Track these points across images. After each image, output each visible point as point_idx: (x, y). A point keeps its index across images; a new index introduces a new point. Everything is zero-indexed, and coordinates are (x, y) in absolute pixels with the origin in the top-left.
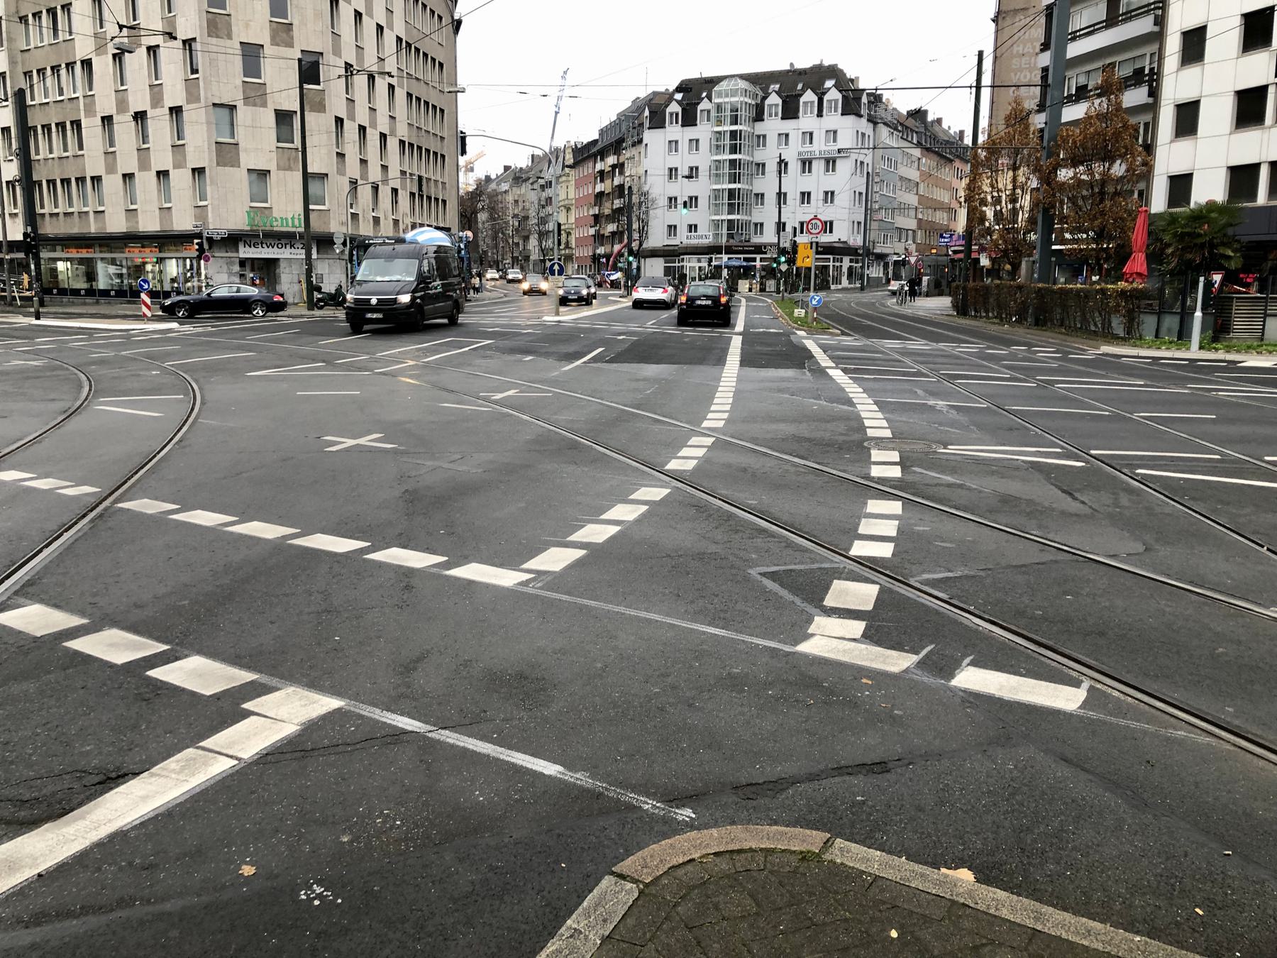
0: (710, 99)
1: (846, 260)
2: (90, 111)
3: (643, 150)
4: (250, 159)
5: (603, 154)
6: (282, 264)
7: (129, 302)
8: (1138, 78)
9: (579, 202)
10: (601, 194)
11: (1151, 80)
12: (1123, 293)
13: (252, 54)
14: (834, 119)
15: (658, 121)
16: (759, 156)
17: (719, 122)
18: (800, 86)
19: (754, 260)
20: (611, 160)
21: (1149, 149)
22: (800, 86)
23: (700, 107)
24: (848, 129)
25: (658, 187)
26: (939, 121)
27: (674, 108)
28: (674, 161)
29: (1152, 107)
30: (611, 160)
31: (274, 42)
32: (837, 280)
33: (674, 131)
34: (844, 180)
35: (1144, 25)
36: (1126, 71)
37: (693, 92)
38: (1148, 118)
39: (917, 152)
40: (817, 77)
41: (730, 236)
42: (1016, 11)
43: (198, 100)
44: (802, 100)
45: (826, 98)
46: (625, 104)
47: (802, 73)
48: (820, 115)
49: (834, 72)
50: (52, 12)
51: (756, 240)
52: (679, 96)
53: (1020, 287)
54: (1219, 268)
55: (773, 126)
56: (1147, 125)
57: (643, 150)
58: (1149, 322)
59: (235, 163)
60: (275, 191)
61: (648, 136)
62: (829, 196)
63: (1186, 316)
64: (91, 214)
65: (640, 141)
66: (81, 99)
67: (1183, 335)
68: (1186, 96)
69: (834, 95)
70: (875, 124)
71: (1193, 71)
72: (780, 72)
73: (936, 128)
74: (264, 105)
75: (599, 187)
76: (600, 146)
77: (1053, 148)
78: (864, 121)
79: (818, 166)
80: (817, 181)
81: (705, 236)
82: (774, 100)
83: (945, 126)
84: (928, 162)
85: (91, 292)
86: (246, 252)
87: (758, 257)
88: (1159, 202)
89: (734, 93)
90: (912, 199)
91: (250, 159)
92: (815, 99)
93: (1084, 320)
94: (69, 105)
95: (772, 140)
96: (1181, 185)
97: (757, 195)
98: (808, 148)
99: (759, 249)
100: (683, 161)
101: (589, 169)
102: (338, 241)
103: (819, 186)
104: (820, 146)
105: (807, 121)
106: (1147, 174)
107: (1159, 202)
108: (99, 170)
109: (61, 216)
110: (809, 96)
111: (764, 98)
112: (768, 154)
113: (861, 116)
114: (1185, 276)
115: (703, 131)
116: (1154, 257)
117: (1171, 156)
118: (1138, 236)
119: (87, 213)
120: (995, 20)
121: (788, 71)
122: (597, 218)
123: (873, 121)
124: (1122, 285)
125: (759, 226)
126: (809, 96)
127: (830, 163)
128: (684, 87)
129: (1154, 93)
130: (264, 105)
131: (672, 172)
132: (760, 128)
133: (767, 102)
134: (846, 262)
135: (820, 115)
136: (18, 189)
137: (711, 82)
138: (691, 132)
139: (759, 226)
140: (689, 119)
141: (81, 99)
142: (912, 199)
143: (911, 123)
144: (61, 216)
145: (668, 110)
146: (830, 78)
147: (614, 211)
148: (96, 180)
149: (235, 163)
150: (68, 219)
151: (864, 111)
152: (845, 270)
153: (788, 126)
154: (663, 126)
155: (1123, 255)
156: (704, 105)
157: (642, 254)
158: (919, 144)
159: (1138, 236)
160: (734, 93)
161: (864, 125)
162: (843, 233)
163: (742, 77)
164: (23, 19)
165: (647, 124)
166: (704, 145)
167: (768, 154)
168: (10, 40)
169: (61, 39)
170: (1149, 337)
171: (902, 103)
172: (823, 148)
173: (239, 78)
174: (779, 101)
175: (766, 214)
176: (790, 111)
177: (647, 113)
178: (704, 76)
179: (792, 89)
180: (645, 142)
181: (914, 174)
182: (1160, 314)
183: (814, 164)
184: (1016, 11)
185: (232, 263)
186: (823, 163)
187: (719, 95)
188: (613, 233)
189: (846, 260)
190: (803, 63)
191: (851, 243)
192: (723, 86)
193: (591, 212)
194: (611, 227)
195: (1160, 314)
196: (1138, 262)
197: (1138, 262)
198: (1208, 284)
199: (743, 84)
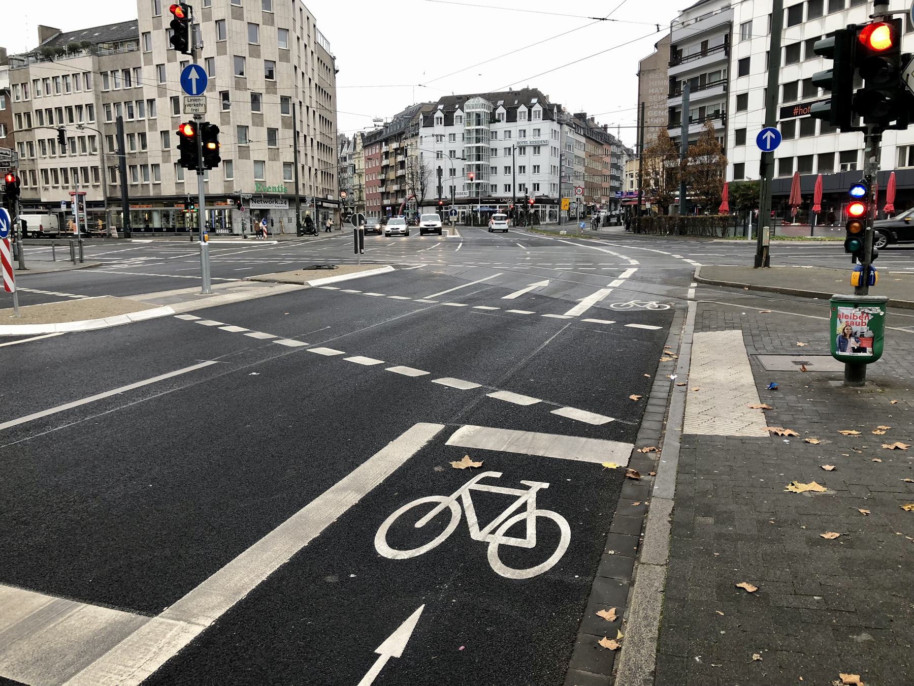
0: (462, 110)
1: (548, 209)
2: (153, 126)
3: (419, 140)
4: (255, 156)
5: (387, 141)
6: (271, 212)
7: (176, 235)
8: (716, 115)
9: (369, 172)
10: (387, 166)
11: (723, 117)
12: (721, 218)
13: (255, 99)
14: (538, 122)
15: (429, 122)
16: (493, 144)
17: (469, 124)
18: (516, 102)
19: (495, 207)
20: (395, 145)
21: (723, 151)
22: (516, 102)
23: (455, 114)
24: (547, 127)
25: (431, 164)
26: (593, 119)
27: (439, 114)
28: (439, 147)
29: (725, 129)
30: (395, 145)
31: (267, 93)
32: (544, 219)
33: (439, 129)
34: (546, 159)
35: (719, 90)
36: (711, 112)
37: (451, 106)
38: (722, 134)
39: (583, 140)
40: (528, 96)
41: (477, 193)
42: (649, 71)
43: (229, 123)
44: (518, 110)
45: (533, 109)
46: (401, 109)
47: (516, 94)
48: (530, 119)
49: (535, 93)
50: (127, 72)
51: (494, 195)
52: (441, 107)
53: (671, 218)
54: (757, 208)
55: (501, 127)
56: (722, 138)
57: (419, 140)
58: (732, 230)
59: (248, 157)
60: (267, 172)
61: (423, 131)
62: (536, 168)
63: (745, 227)
64: (151, 186)
65: (417, 134)
66: (147, 122)
67: (745, 234)
68: (740, 126)
69: (538, 108)
70: (561, 124)
71: (744, 79)
72: (503, 93)
73: (591, 123)
74: (262, 125)
75: (385, 162)
76: (384, 136)
77: (671, 148)
78: (555, 123)
79: (529, 150)
80: (528, 159)
81: (462, 193)
82: (501, 110)
83: (596, 122)
84: (591, 147)
85: (148, 229)
86: (253, 206)
87: (498, 205)
88: (729, 177)
89: (476, 106)
90: (581, 169)
91: (255, 156)
92: (527, 110)
93: (704, 230)
94: (137, 125)
95: (501, 135)
96: (739, 169)
97: (492, 168)
98: (522, 139)
99: (498, 201)
100: (445, 146)
101: (375, 150)
102: (308, 200)
103: (531, 163)
104: (530, 138)
105: (522, 123)
106: (725, 163)
107: (729, 177)
108: (158, 160)
109: (140, 187)
110: (523, 108)
111: (495, 109)
112: (500, 144)
113: (553, 120)
114: (745, 210)
115: (458, 128)
116: (732, 204)
117: (734, 154)
118: (724, 195)
119: (147, 185)
120: (639, 75)
121: (508, 93)
122: (383, 182)
123: (560, 123)
124: (720, 215)
125: (494, 187)
126: (523, 108)
127: (537, 148)
128: (443, 100)
129: (725, 123)
130: (262, 125)
131: (439, 155)
132: (495, 127)
133: (497, 112)
134: (548, 209)
135: (530, 119)
136: (117, 172)
137: (461, 100)
138: (450, 130)
139: (494, 187)
140: (449, 121)
141: (147, 122)
142: (581, 169)
143: (577, 121)
144: (140, 187)
145: (435, 116)
146: (534, 97)
147: (397, 178)
148: (156, 166)
149: (248, 157)
150: (134, 189)
151: (555, 117)
152: (547, 213)
153: (511, 126)
154: (432, 126)
155: (718, 203)
156: (458, 113)
157: (422, 204)
158: (584, 135)
159: (724, 195)
160: (476, 106)
161: (555, 125)
162: (544, 191)
163: (480, 95)
164: (105, 74)
165: (422, 124)
166: (459, 137)
167: (500, 144)
168: (95, 85)
169: (133, 86)
170: (732, 236)
171: (571, 109)
172: (532, 139)
173: (250, 112)
174: (505, 111)
175: (500, 180)
176: (512, 117)
177: (421, 117)
178: (455, 94)
179: (513, 103)
180: (420, 135)
181: (582, 154)
182: (735, 226)
183: (527, 149)
184: (649, 71)
185: (246, 212)
186: (532, 148)
187: (469, 107)
188: (397, 192)
189: (548, 206)
190: (517, 88)
191: (551, 196)
192: (471, 102)
193: (380, 178)
194: (395, 187)
195: (735, 226)
196: (725, 206)
197: (725, 206)
198: (754, 214)
199: (482, 101)
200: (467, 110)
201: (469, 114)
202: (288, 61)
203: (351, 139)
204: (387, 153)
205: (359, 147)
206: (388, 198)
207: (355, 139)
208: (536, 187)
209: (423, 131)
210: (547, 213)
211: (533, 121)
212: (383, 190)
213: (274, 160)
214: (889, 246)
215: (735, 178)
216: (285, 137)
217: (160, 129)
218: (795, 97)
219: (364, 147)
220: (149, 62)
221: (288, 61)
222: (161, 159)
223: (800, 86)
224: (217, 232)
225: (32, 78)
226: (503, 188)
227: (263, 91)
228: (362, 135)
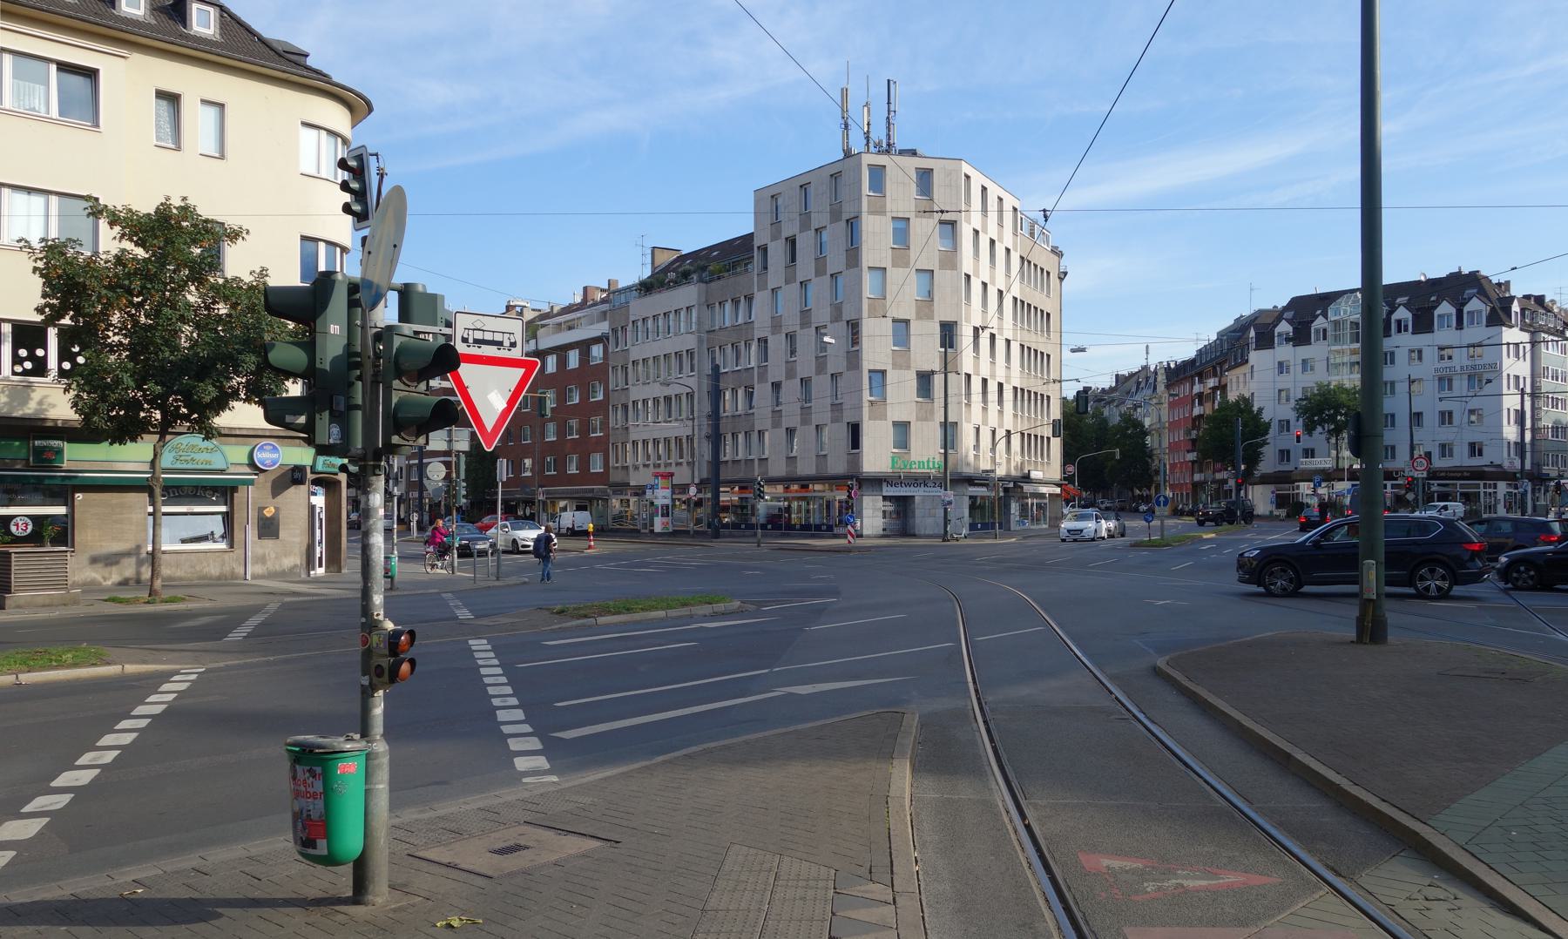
5: (1202, 377)
15: (1266, 340)
20: (1211, 382)
26: (1260, 410)
27: (1284, 327)
30: (1211, 382)
33: (1284, 352)
44: (1437, 312)
45: (1466, 309)
46: (1227, 322)
48: (1460, 326)
61: (1255, 356)
74: (908, 367)
75: (1197, 411)
82: (1402, 314)
92: (1453, 311)
101: (1183, 390)
105: (1444, 335)
126: (1446, 308)
133: (1395, 317)
135: (1460, 326)
138: (1304, 352)
146: (1472, 287)
153: (1422, 340)
156: (1320, 323)
176: (1423, 323)
177: (1252, 333)
200: (1332, 317)
201: (1336, 323)
204: (1200, 395)
205: (1161, 388)
206: (1201, 471)
208: (1445, 449)
209: (1255, 356)
210: (1500, 496)
211: (1466, 329)
213: (926, 419)
214: (1306, 589)
217: (771, 380)
219: (1168, 387)
220: (762, 287)
222: (769, 421)
224: (836, 531)
225: (632, 318)
226: (1466, 450)
227: (797, 328)
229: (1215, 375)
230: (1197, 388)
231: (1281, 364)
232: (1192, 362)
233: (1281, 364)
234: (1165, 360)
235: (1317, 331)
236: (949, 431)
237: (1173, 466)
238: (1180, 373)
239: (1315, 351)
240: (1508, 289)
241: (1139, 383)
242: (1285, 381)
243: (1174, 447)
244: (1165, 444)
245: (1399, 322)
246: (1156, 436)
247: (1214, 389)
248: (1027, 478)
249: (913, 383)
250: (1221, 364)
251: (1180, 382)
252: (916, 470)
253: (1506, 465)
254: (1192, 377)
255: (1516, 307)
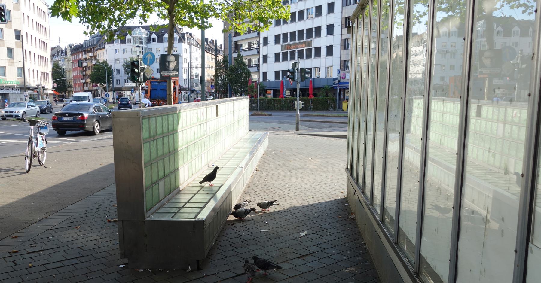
15: (111, 41)
20: (90, 54)
26: (111, 66)
30: (90, 54)
33: (117, 45)
61: (107, 46)
82: (154, 36)
101: (78, 57)
111: (150, 35)
130: (4, 46)
133: (152, 37)
138: (123, 46)
156: (128, 37)
200: (133, 36)
201: (134, 37)
202: (19, 10)
203: (64, 49)
204: (86, 59)
206: (87, 86)
207: (66, 49)
209: (107, 46)
210: (182, 96)
212: (83, 81)
215: (275, 79)
216: (18, 53)
218: (287, 41)
219: (72, 55)
221: (19, 10)
223: (314, 30)
228: (71, 47)
229: (91, 52)
230: (84, 56)
231: (116, 50)
232: (82, 46)
233: (116, 50)
234: (70, 43)
235: (128, 39)
236: (22, 70)
237: (75, 85)
238: (76, 50)
239: (128, 46)
240: (182, 31)
241: (58, 53)
242: (118, 56)
243: (75, 77)
244: (71, 76)
245: (153, 39)
246: (68, 73)
247: (91, 57)
248: (44, 88)
249: (6, 51)
250: (94, 48)
251: (76, 53)
252: (10, 84)
253: (184, 86)
254: (82, 52)
255: (186, 37)
